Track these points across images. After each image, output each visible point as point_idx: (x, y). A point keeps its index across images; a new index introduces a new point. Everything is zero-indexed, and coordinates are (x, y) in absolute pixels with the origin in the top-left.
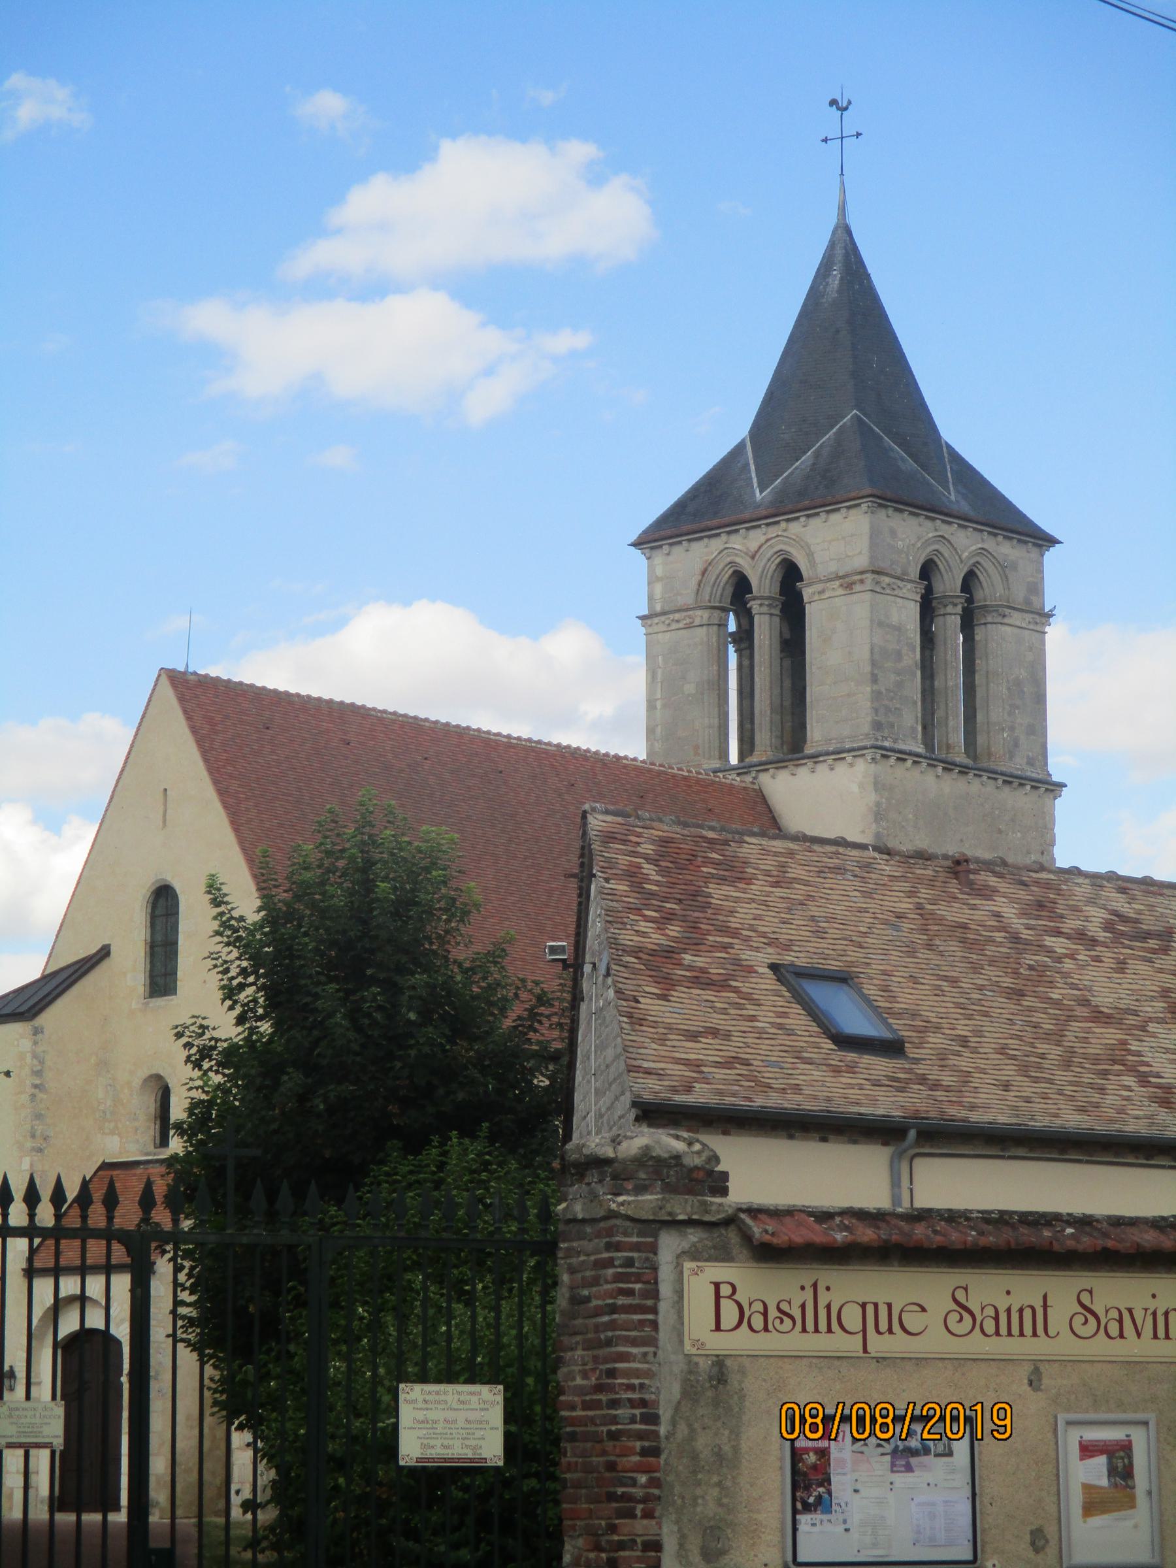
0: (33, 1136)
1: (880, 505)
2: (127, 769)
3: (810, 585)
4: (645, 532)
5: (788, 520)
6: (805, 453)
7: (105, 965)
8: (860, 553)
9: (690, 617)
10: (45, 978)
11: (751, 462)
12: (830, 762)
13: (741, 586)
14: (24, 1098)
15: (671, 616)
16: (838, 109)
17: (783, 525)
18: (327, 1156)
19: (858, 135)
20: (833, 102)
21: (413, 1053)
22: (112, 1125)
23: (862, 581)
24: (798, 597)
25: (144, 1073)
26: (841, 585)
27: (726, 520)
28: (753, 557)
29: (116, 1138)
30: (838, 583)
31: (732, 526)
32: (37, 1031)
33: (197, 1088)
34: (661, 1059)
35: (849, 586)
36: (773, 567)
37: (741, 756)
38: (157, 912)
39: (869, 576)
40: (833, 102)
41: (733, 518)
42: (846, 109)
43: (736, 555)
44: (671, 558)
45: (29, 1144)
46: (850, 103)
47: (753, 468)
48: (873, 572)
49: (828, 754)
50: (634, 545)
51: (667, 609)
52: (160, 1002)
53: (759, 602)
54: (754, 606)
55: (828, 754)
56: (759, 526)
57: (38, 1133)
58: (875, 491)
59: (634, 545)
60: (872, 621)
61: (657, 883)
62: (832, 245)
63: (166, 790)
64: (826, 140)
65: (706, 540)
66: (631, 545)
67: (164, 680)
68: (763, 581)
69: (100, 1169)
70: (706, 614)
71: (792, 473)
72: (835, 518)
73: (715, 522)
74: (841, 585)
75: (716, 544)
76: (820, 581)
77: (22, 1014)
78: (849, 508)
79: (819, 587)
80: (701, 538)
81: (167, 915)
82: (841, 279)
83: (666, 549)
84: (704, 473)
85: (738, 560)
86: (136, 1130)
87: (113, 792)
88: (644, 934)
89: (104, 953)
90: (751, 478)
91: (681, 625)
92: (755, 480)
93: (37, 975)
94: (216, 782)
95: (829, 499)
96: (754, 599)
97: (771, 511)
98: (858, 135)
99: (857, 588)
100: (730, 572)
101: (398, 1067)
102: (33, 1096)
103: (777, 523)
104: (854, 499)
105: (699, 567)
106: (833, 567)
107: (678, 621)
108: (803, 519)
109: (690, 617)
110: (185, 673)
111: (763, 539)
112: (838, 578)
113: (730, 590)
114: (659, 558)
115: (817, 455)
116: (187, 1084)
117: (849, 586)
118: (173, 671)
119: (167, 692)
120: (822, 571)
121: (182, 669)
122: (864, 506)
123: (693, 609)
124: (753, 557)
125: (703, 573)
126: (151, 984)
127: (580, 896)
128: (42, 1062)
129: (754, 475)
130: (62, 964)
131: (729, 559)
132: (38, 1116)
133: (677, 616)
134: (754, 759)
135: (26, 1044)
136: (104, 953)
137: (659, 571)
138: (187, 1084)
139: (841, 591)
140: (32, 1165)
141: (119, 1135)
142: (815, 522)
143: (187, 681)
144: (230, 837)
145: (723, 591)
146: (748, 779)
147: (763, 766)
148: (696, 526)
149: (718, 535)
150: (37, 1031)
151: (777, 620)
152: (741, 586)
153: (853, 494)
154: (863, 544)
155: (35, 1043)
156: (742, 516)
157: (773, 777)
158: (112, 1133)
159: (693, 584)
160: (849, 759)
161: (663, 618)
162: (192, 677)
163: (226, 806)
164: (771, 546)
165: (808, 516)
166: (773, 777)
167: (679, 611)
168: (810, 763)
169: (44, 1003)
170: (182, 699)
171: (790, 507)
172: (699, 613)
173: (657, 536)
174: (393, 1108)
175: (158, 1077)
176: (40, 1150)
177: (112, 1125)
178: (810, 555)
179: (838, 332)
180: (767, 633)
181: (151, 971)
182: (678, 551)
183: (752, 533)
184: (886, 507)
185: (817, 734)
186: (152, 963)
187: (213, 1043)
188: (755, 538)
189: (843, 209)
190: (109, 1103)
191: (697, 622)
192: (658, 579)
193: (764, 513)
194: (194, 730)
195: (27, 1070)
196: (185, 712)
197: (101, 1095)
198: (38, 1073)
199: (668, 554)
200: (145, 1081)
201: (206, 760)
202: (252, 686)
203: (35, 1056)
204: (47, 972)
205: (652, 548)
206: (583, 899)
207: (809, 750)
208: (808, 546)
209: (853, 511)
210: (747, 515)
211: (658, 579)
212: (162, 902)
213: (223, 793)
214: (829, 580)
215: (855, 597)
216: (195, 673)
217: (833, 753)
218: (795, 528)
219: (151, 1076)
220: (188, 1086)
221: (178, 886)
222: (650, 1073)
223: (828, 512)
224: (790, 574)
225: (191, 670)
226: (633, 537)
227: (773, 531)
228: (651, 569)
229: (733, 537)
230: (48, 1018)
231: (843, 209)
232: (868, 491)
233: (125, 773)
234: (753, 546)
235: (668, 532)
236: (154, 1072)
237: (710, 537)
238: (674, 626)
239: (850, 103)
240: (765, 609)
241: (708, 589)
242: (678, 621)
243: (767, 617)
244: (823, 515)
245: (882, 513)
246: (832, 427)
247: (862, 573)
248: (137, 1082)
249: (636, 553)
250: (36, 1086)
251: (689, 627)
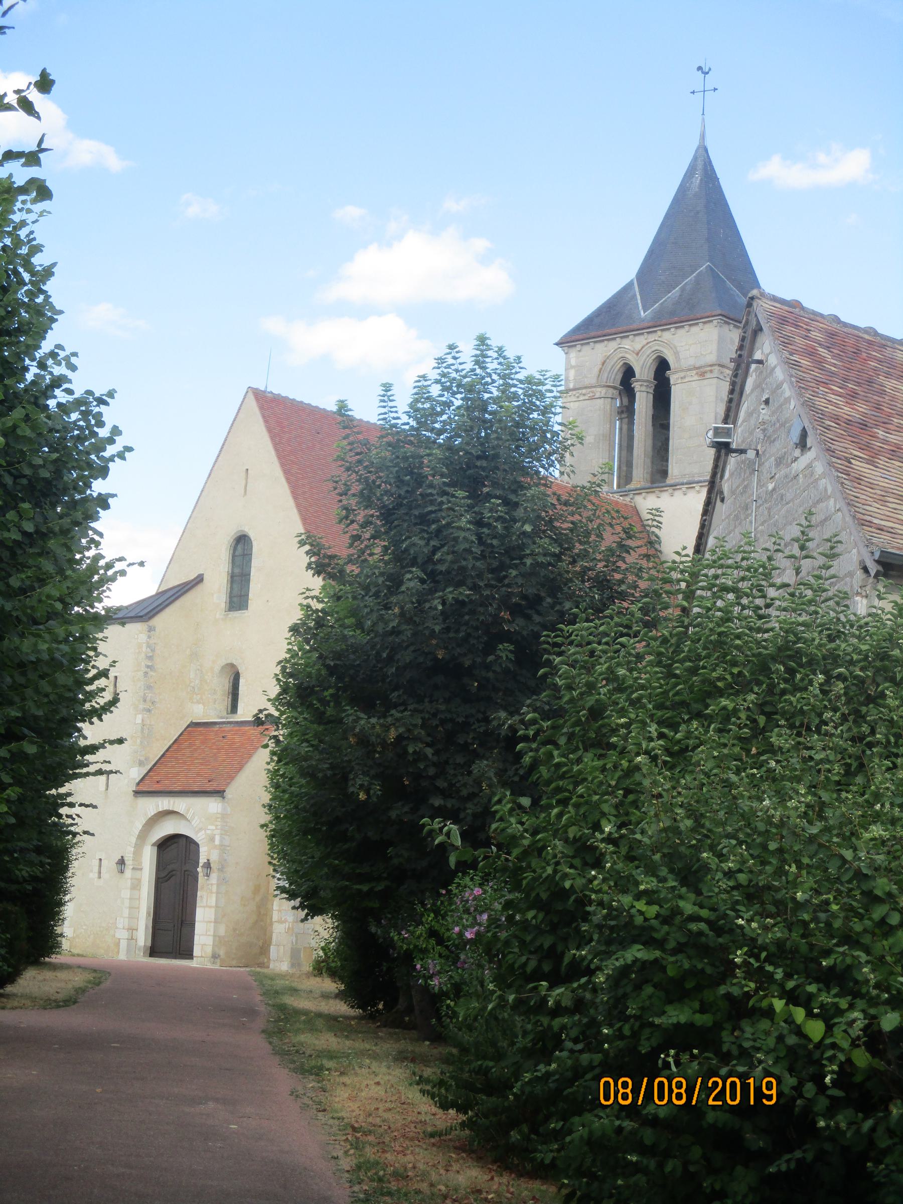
0: (145, 701)
1: (726, 323)
2: (222, 455)
3: (676, 372)
4: (565, 336)
5: (662, 330)
6: (674, 288)
7: (200, 586)
8: (711, 353)
9: (592, 392)
10: (159, 594)
11: (638, 294)
12: (684, 489)
13: (628, 373)
14: (141, 674)
15: (580, 391)
16: (703, 72)
17: (659, 333)
18: (440, 657)
19: (715, 89)
20: (700, 68)
21: (528, 561)
22: (199, 697)
23: (711, 371)
24: (667, 380)
25: (222, 662)
26: (697, 374)
27: (620, 329)
28: (637, 354)
29: (201, 706)
30: (695, 372)
31: (625, 333)
32: (151, 629)
33: (312, 598)
34: (888, 518)
35: (702, 374)
36: (651, 361)
37: (619, 486)
38: (237, 553)
39: (717, 368)
40: (700, 68)
41: (625, 328)
42: (707, 73)
43: (626, 352)
44: (581, 354)
45: (141, 706)
46: (710, 69)
47: (639, 297)
48: (720, 365)
49: (683, 484)
50: (557, 344)
51: (577, 386)
52: (237, 614)
53: (640, 383)
54: (636, 386)
55: (683, 484)
56: (643, 334)
57: (148, 699)
58: (723, 313)
59: (557, 344)
60: (716, 397)
61: (834, 365)
62: (695, 158)
63: (100, 860)
64: (693, 92)
65: (606, 342)
66: (557, 344)
67: (251, 396)
68: (644, 371)
69: (188, 726)
70: (604, 390)
71: (666, 301)
72: (695, 329)
73: (613, 330)
74: (697, 374)
75: (613, 345)
76: (682, 371)
77: (141, 617)
78: (704, 323)
79: (682, 374)
80: (603, 341)
81: (244, 555)
82: (701, 180)
83: (579, 347)
84: (605, 300)
85: (627, 356)
86: (215, 701)
87: (211, 470)
88: (836, 405)
89: (199, 580)
90: (637, 304)
91: (587, 397)
92: (640, 305)
93: (153, 592)
94: (282, 465)
95: (692, 316)
96: (637, 381)
97: (650, 324)
98: (715, 89)
99: (708, 375)
100: (621, 364)
101: (513, 575)
102: (146, 673)
103: (655, 331)
104: (708, 317)
105: (600, 360)
106: (691, 362)
107: (584, 395)
108: (672, 330)
109: (592, 392)
110: (264, 392)
111: (645, 342)
112: (697, 368)
113: (619, 377)
114: (573, 354)
115: (683, 289)
116: (304, 593)
117: (702, 374)
118: (257, 389)
119: (252, 402)
120: (684, 364)
121: (263, 389)
122: (715, 322)
123: (595, 387)
124: (637, 354)
125: (603, 364)
126: (230, 602)
127: (732, 392)
128: (153, 650)
129: (639, 301)
130: (171, 586)
131: (621, 355)
132: (149, 687)
133: (584, 391)
134: (632, 486)
135: (143, 637)
136: (199, 579)
137: (573, 362)
138: (304, 593)
139: (696, 378)
140: (143, 720)
141: (203, 704)
142: (681, 332)
143: (265, 397)
144: (291, 503)
145: (616, 378)
146: (628, 499)
147: (638, 491)
148: (599, 333)
149: (614, 339)
150: (151, 629)
151: (651, 396)
152: (628, 373)
153: (706, 314)
154: (713, 347)
155: (149, 637)
156: (632, 327)
157: (644, 498)
158: (198, 702)
159: (596, 370)
160: (697, 488)
161: (574, 393)
162: (270, 395)
163: (288, 480)
164: (650, 347)
165: (677, 328)
166: (644, 498)
167: (585, 388)
168: (670, 490)
169: (154, 612)
170: (261, 408)
171: (664, 321)
172: (599, 389)
173: (573, 338)
174: (505, 615)
175: (232, 666)
176: (149, 711)
177: (199, 697)
178: (676, 354)
179: (698, 213)
180: (644, 403)
181: (231, 592)
182: (586, 349)
183: (638, 338)
184: (729, 324)
185: (675, 469)
186: (232, 588)
187: (327, 561)
188: (638, 342)
189: (703, 137)
190: (197, 682)
191: (597, 395)
192: (572, 367)
193: (646, 325)
194: (270, 430)
195: (143, 655)
196: (264, 416)
197: (192, 676)
198: (150, 658)
199: (579, 351)
200: (223, 668)
201: (276, 450)
202: (309, 405)
203: (148, 646)
204: (160, 590)
205: (569, 347)
206: (735, 396)
207: (669, 481)
208: (676, 348)
209: (707, 326)
210: (635, 326)
211: (572, 367)
212: (240, 547)
213: (287, 473)
214: (690, 370)
215: (706, 382)
216: (272, 393)
217: (687, 484)
218: (667, 336)
219: (227, 664)
220: (304, 596)
221: (252, 535)
222: (882, 530)
223: (690, 325)
224: (662, 366)
225: (268, 390)
226: (557, 340)
227: (652, 337)
228: (568, 361)
229: (625, 341)
230: (159, 621)
231: (703, 137)
232: (719, 312)
233: (220, 458)
234: (638, 347)
235: (581, 337)
236: (229, 662)
237: (608, 340)
238: (582, 398)
239: (710, 69)
240: (644, 389)
241: (606, 375)
242: (584, 395)
243: (645, 394)
244: (687, 328)
245: (726, 327)
246: (693, 272)
247: (711, 366)
248: (217, 668)
249: (558, 349)
250: (148, 667)
251: (591, 398)
